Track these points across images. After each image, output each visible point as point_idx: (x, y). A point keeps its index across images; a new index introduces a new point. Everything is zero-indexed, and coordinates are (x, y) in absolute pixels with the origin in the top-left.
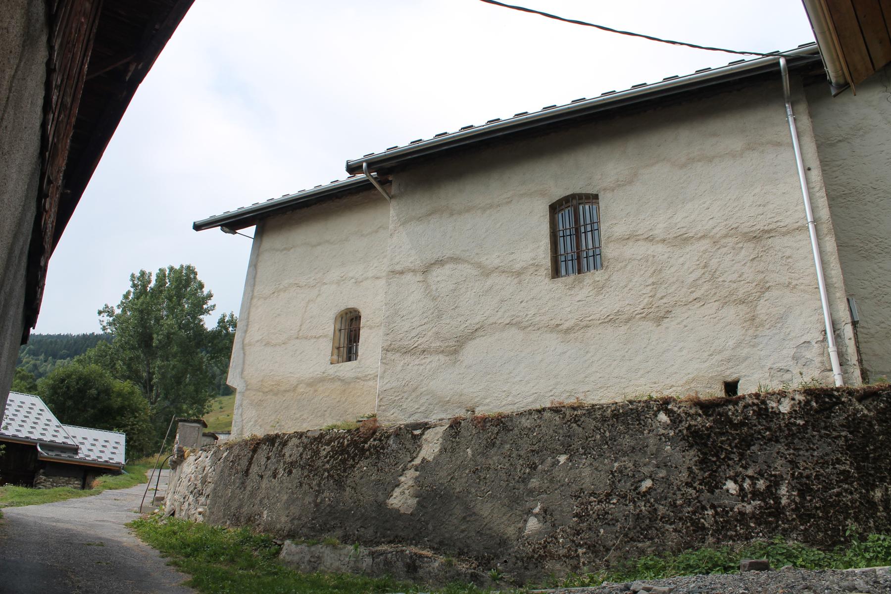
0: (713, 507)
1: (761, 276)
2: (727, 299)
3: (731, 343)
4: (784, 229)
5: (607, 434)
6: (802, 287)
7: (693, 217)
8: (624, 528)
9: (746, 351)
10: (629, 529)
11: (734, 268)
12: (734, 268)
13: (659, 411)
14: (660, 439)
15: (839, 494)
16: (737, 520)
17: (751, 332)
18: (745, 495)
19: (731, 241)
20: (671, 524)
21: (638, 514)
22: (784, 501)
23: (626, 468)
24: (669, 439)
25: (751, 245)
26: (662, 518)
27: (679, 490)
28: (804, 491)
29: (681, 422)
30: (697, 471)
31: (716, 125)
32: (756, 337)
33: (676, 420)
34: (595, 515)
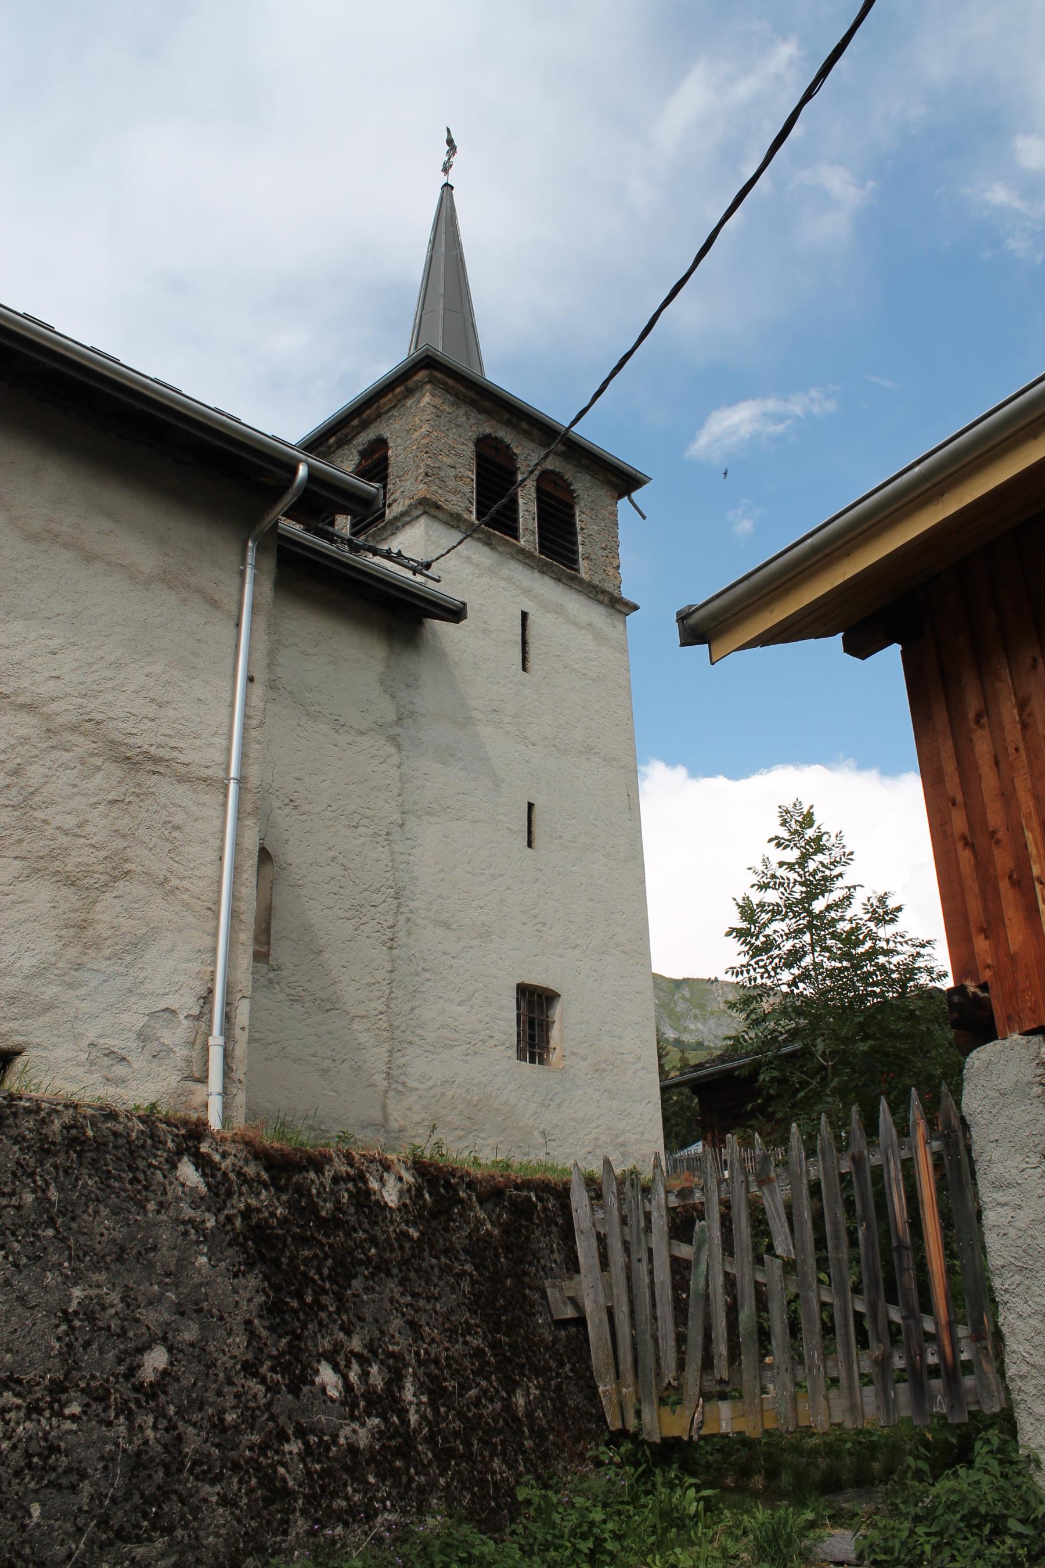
0: (301, 1433)
1: (118, 844)
2: (42, 864)
3: (27, 963)
4: (183, 770)
5: (54, 1194)
6: (185, 897)
7: (18, 654)
8: (102, 1496)
9: (52, 990)
10: (114, 1500)
11: (73, 804)
12: (73, 804)
13: (180, 1153)
14: (186, 1233)
15: (477, 1403)
16: (347, 1469)
17: (72, 953)
18: (354, 1405)
19: (84, 745)
20: (213, 1483)
21: (138, 1454)
22: (413, 1418)
23: (104, 1308)
24: (207, 1237)
25: (118, 771)
26: (196, 1463)
27: (230, 1382)
28: (435, 1392)
29: (229, 1194)
30: (264, 1333)
31: (117, 497)
32: (79, 967)
33: (220, 1187)
34: (16, 1455)
